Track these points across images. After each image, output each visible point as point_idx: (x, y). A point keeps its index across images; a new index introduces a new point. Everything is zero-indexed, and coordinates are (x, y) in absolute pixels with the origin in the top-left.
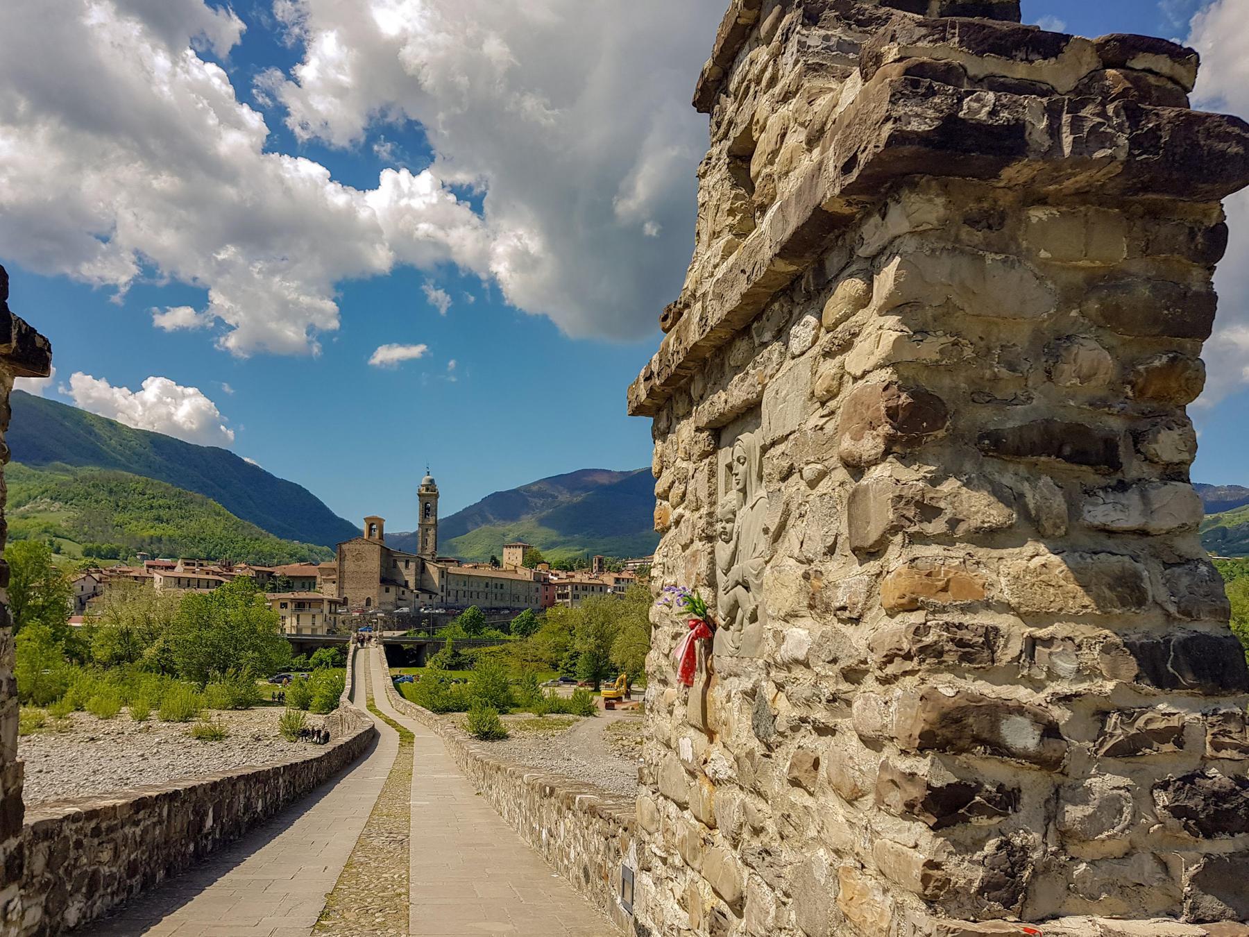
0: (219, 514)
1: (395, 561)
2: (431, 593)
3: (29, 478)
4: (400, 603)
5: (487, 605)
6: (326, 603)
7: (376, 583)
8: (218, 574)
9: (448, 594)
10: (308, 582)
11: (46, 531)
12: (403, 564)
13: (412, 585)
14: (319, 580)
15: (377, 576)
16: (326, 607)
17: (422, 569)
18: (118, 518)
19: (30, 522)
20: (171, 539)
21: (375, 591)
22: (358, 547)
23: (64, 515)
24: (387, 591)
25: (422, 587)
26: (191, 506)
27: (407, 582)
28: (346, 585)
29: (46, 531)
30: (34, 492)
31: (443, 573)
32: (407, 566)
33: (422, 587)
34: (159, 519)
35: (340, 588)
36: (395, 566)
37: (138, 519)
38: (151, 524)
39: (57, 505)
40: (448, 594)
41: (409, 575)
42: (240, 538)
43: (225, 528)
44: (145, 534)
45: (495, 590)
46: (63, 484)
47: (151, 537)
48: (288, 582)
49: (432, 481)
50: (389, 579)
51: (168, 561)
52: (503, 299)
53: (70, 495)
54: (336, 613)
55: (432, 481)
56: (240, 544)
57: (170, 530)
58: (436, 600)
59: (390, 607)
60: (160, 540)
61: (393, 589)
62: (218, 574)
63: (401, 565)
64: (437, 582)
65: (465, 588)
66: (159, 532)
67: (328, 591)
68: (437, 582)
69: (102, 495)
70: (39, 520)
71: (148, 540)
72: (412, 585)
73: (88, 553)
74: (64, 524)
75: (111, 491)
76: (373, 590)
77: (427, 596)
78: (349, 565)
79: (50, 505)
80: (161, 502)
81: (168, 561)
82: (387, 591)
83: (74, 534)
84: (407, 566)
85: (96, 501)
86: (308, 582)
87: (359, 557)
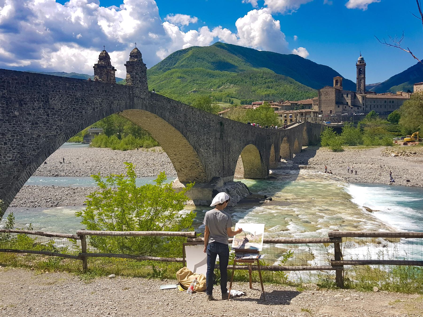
0: (291, 83)
1: (342, 94)
2: (358, 107)
3: (223, 76)
4: (344, 111)
5: (386, 110)
6: (312, 113)
7: (334, 104)
8: (277, 105)
9: (367, 107)
10: (309, 106)
11: (228, 96)
12: (346, 95)
13: (349, 104)
14: (313, 105)
15: (334, 101)
16: (312, 115)
17: (354, 97)
18: (253, 88)
19: (223, 93)
20: (273, 95)
21: (333, 107)
22: (326, 90)
23: (235, 89)
24: (339, 107)
25: (355, 104)
26: (280, 81)
27: (347, 103)
28: (322, 106)
29: (228, 96)
30: (224, 81)
31: (364, 98)
32: (347, 96)
33: (355, 104)
34: (268, 87)
35: (320, 107)
36: (342, 96)
37: (260, 88)
38: (265, 89)
39: (232, 85)
40: (367, 107)
41: (349, 100)
42: (300, 92)
43: (294, 89)
44: (263, 94)
45: (389, 104)
46: (234, 77)
47: (266, 95)
48: (303, 106)
49: (362, 59)
50: (339, 101)
51: (260, 102)
52: (282, 13)
53: (236, 81)
54: (316, 116)
55: (362, 59)
56: (300, 94)
57: (273, 91)
58: (361, 109)
59: (340, 114)
60: (269, 95)
61: (341, 106)
62: (277, 105)
63: (345, 96)
64: (361, 102)
65: (374, 104)
66: (268, 92)
67: (316, 108)
68: (361, 102)
69: (248, 80)
70: (226, 92)
71: (264, 96)
72: (349, 104)
73: (242, 103)
74: (234, 93)
75: (250, 78)
76: (333, 107)
77: (356, 108)
78: (323, 97)
79: (230, 86)
80: (269, 80)
81: (260, 102)
82: (339, 107)
83: (238, 96)
84: (347, 96)
85: (245, 82)
86: (309, 106)
87: (327, 94)
